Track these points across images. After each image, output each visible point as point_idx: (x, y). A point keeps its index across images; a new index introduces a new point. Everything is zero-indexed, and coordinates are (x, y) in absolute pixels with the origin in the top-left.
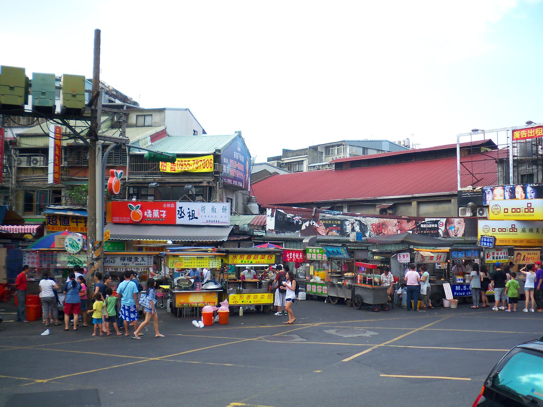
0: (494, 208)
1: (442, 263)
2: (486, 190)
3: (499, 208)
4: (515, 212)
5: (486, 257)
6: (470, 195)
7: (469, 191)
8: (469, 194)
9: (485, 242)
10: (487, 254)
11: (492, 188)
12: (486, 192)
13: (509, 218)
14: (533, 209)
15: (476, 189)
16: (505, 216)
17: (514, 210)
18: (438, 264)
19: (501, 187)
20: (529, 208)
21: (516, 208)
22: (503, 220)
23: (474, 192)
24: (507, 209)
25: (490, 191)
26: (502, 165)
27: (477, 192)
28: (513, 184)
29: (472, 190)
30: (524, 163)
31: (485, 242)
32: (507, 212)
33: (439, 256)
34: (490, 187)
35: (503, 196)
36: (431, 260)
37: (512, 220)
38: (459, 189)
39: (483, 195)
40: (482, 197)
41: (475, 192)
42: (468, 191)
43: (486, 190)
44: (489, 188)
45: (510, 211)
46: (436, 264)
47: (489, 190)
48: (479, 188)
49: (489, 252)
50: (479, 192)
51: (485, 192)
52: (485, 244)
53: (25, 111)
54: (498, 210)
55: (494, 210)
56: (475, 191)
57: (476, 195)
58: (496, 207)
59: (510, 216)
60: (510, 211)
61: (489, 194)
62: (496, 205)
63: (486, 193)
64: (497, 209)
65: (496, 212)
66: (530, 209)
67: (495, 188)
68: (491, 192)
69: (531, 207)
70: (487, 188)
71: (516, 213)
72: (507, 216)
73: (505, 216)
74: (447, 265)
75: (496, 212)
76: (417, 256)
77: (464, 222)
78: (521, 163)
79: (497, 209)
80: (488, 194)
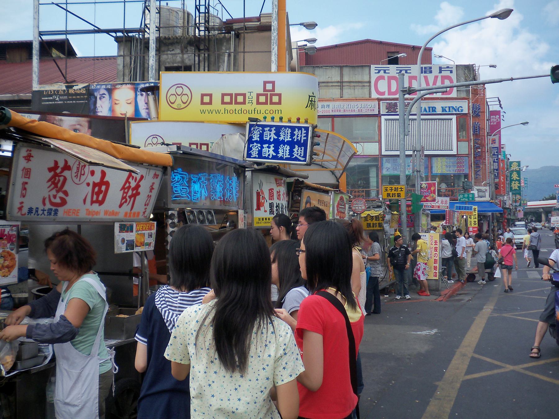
0: (172, 91)
1: (138, 222)
2: (97, 90)
3: (186, 91)
4: (231, 103)
5: (255, 207)
6: (60, 100)
7: (58, 91)
8: (57, 99)
9: (269, 142)
10: (258, 194)
11: (109, 87)
12: (96, 94)
13: (214, 117)
14: (280, 95)
15: (75, 88)
16: (203, 112)
17: (227, 99)
18: (123, 228)
19: (129, 86)
20: (269, 93)
21: (234, 92)
22: (203, 122)
23: (68, 94)
24: (210, 95)
25: (106, 92)
26: (129, 44)
27: (76, 94)
28: (153, 81)
29: (64, 91)
30: (172, 44)
31: (269, 142)
32: (210, 103)
33: (133, 184)
34: (106, 85)
35: (133, 104)
36: (96, 206)
37: (221, 123)
38: (36, 87)
39: (89, 101)
40: (87, 104)
41: (72, 95)
42: (56, 93)
43: (97, 90)
44: (104, 87)
45: (217, 99)
46: (117, 226)
47: (103, 91)
48: (81, 86)
49: (261, 185)
50: (83, 94)
51: (94, 95)
52: (269, 151)
53: (146, 340)
54: (185, 98)
55: (172, 99)
56: (71, 91)
57: (73, 100)
58: (179, 91)
59: (218, 112)
60: (217, 99)
61: (103, 100)
62: (180, 85)
63: (96, 98)
64: (182, 94)
65: (179, 101)
66: (272, 95)
67: (117, 87)
68: (107, 96)
69: (273, 90)
70: (99, 87)
71: (233, 107)
72: (211, 112)
73: (203, 112)
74: (154, 231)
75: (179, 101)
76: (27, 172)
77: (90, 127)
78: (166, 45)
79: (182, 94)
80: (100, 99)
